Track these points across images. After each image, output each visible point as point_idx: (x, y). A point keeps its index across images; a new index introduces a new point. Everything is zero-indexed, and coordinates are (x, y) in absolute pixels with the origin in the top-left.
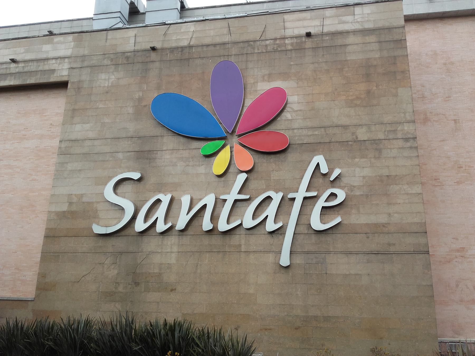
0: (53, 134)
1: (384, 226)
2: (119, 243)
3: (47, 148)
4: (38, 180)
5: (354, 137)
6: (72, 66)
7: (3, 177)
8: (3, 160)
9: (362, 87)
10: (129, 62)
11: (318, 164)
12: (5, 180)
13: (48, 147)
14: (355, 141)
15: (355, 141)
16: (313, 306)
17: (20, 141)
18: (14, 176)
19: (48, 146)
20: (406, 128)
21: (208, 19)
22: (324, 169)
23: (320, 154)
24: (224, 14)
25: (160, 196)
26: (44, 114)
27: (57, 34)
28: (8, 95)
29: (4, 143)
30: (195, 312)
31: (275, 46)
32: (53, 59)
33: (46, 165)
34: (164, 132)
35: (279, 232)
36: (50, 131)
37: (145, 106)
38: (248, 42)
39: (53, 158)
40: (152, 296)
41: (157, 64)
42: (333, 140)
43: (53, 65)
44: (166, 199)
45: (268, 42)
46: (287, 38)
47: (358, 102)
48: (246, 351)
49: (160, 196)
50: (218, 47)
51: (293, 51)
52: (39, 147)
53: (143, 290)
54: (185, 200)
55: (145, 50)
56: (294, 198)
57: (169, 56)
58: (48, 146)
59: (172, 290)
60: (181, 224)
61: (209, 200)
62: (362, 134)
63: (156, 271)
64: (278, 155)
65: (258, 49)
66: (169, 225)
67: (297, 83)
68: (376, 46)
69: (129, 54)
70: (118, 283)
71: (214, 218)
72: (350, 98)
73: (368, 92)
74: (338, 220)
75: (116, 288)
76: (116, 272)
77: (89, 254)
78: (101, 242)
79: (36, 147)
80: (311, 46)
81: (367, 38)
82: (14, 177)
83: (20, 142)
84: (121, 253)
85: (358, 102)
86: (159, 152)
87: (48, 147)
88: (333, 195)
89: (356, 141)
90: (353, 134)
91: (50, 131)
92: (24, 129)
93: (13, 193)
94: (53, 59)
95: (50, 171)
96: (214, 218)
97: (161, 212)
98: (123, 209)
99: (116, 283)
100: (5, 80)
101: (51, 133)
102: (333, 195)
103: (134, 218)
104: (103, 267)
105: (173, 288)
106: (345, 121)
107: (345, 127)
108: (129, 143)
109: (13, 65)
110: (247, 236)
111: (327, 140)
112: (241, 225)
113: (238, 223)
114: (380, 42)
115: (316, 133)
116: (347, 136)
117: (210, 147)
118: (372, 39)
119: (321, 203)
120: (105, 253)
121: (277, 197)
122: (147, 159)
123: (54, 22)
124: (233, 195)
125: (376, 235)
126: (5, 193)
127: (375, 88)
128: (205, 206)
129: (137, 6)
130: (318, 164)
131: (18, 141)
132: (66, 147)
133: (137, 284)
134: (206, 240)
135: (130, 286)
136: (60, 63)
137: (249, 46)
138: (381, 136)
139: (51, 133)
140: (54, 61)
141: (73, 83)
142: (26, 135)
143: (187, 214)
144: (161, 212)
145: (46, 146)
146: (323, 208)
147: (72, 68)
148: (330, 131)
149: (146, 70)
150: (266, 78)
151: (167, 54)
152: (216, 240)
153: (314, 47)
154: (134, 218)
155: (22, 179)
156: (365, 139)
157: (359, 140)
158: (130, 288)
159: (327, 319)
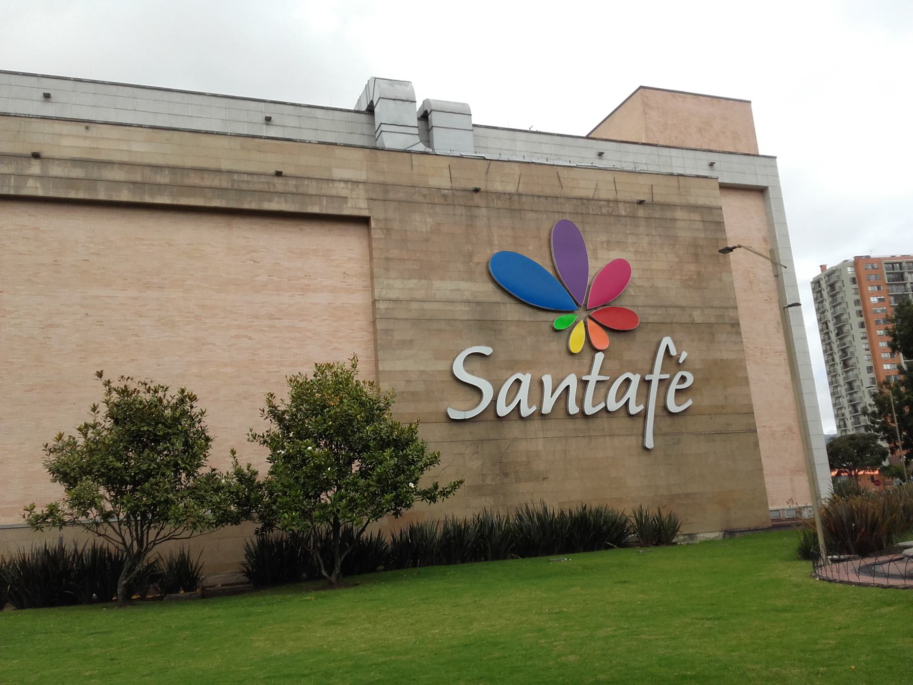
0: (350, 287)
1: (723, 408)
2: (479, 430)
3: (344, 305)
4: (342, 349)
5: (691, 319)
6: (371, 196)
7: (288, 343)
8: (281, 319)
9: (692, 267)
10: (448, 203)
11: (667, 346)
12: (292, 348)
13: (346, 305)
14: (692, 324)
15: (692, 324)
16: (674, 485)
17: (302, 293)
18: (304, 342)
19: (346, 304)
20: (731, 314)
21: (534, 163)
22: (673, 352)
23: (669, 336)
24: (546, 156)
25: (518, 376)
26: (331, 258)
27: (339, 144)
28: (268, 222)
29: (278, 294)
30: (571, 499)
31: (610, 209)
32: (340, 181)
33: (349, 330)
34: (506, 299)
35: (644, 415)
36: (345, 282)
37: (478, 264)
38: (581, 199)
39: (357, 320)
40: (525, 487)
41: (484, 211)
42: (674, 321)
43: (341, 189)
44: (526, 379)
45: (602, 203)
46: (620, 202)
47: (691, 283)
48: (53, 553)
49: (518, 376)
50: (550, 200)
51: (627, 218)
52: (333, 303)
53: (514, 481)
54: (547, 380)
55: (465, 190)
56: (601, 375)
57: (499, 203)
58: (346, 304)
59: (544, 479)
60: (547, 408)
61: (571, 381)
62: (698, 317)
63: (524, 459)
64: (616, 334)
65: (593, 211)
66: (534, 408)
67: (636, 256)
68: (699, 225)
69: (446, 192)
70: (485, 475)
71: (580, 402)
72: (684, 278)
73: (699, 273)
74: (689, 403)
75: (484, 481)
76: (480, 463)
77: (444, 444)
78: (456, 429)
79: (329, 303)
80: (643, 216)
81: (692, 215)
82: (306, 344)
83: (303, 295)
84: (482, 441)
85: (691, 283)
86: (504, 323)
87: (346, 305)
88: (683, 379)
89: (693, 323)
90: (690, 316)
91: (345, 282)
92: (305, 276)
93: (310, 367)
94: (340, 181)
95: (357, 338)
96: (580, 402)
97: (523, 394)
98: (478, 391)
99: (482, 475)
100: (270, 201)
101: (347, 285)
102: (683, 379)
103: (494, 401)
104: (464, 457)
105: (545, 477)
106: (682, 302)
107: (682, 308)
108: (467, 308)
109: (277, 180)
110: (609, 419)
111: (669, 321)
112: (606, 407)
113: (602, 405)
114: (703, 221)
115: (659, 312)
116: (685, 319)
117: (560, 321)
118: (696, 217)
119: (674, 386)
120: (463, 442)
121: (636, 379)
122: (492, 330)
123: (208, 95)
124: (593, 378)
125: (717, 416)
126: (296, 366)
127: (703, 270)
128: (568, 387)
129: (375, 105)
130: (667, 346)
131: (300, 293)
132: (386, 309)
133: (506, 475)
134: (570, 425)
135: (499, 478)
136: (352, 190)
137: (582, 204)
138: (713, 320)
139: (347, 285)
140: (342, 185)
141: (378, 220)
142: (309, 285)
143: (551, 397)
144: (523, 394)
145: (343, 304)
146: (677, 390)
147: (372, 199)
148: (671, 311)
149: (472, 217)
150: (605, 245)
151: (493, 200)
152: (580, 424)
153: (646, 216)
154: (494, 401)
155: (318, 348)
156: (701, 322)
157: (695, 322)
158: (500, 480)
159: (687, 496)
